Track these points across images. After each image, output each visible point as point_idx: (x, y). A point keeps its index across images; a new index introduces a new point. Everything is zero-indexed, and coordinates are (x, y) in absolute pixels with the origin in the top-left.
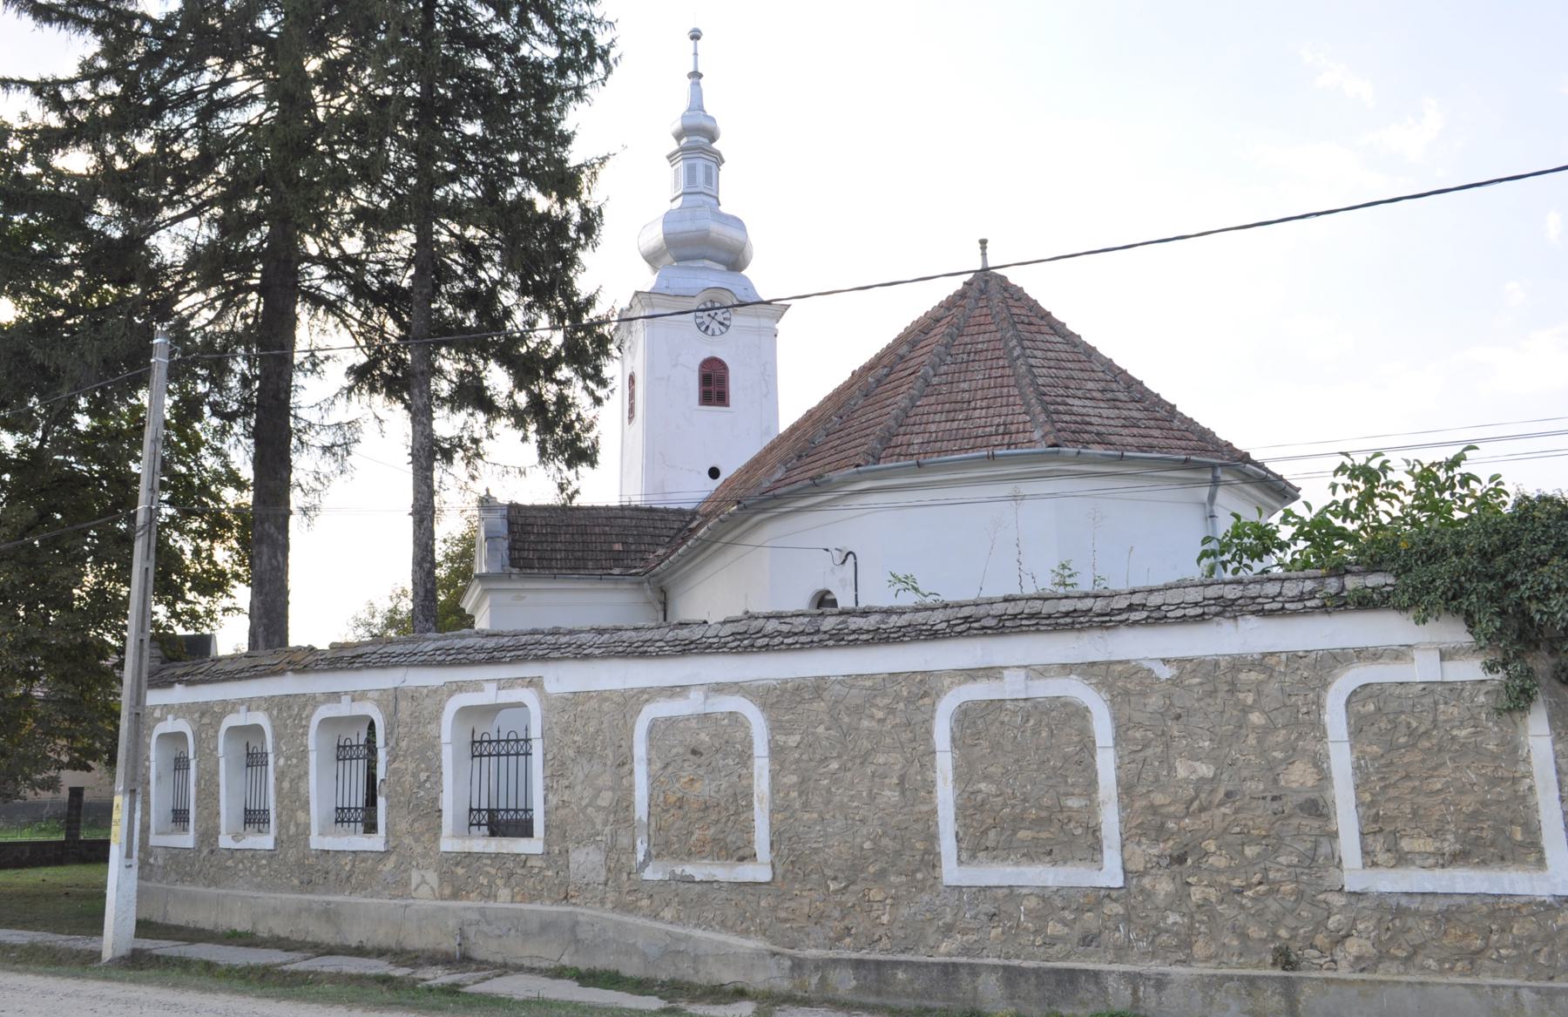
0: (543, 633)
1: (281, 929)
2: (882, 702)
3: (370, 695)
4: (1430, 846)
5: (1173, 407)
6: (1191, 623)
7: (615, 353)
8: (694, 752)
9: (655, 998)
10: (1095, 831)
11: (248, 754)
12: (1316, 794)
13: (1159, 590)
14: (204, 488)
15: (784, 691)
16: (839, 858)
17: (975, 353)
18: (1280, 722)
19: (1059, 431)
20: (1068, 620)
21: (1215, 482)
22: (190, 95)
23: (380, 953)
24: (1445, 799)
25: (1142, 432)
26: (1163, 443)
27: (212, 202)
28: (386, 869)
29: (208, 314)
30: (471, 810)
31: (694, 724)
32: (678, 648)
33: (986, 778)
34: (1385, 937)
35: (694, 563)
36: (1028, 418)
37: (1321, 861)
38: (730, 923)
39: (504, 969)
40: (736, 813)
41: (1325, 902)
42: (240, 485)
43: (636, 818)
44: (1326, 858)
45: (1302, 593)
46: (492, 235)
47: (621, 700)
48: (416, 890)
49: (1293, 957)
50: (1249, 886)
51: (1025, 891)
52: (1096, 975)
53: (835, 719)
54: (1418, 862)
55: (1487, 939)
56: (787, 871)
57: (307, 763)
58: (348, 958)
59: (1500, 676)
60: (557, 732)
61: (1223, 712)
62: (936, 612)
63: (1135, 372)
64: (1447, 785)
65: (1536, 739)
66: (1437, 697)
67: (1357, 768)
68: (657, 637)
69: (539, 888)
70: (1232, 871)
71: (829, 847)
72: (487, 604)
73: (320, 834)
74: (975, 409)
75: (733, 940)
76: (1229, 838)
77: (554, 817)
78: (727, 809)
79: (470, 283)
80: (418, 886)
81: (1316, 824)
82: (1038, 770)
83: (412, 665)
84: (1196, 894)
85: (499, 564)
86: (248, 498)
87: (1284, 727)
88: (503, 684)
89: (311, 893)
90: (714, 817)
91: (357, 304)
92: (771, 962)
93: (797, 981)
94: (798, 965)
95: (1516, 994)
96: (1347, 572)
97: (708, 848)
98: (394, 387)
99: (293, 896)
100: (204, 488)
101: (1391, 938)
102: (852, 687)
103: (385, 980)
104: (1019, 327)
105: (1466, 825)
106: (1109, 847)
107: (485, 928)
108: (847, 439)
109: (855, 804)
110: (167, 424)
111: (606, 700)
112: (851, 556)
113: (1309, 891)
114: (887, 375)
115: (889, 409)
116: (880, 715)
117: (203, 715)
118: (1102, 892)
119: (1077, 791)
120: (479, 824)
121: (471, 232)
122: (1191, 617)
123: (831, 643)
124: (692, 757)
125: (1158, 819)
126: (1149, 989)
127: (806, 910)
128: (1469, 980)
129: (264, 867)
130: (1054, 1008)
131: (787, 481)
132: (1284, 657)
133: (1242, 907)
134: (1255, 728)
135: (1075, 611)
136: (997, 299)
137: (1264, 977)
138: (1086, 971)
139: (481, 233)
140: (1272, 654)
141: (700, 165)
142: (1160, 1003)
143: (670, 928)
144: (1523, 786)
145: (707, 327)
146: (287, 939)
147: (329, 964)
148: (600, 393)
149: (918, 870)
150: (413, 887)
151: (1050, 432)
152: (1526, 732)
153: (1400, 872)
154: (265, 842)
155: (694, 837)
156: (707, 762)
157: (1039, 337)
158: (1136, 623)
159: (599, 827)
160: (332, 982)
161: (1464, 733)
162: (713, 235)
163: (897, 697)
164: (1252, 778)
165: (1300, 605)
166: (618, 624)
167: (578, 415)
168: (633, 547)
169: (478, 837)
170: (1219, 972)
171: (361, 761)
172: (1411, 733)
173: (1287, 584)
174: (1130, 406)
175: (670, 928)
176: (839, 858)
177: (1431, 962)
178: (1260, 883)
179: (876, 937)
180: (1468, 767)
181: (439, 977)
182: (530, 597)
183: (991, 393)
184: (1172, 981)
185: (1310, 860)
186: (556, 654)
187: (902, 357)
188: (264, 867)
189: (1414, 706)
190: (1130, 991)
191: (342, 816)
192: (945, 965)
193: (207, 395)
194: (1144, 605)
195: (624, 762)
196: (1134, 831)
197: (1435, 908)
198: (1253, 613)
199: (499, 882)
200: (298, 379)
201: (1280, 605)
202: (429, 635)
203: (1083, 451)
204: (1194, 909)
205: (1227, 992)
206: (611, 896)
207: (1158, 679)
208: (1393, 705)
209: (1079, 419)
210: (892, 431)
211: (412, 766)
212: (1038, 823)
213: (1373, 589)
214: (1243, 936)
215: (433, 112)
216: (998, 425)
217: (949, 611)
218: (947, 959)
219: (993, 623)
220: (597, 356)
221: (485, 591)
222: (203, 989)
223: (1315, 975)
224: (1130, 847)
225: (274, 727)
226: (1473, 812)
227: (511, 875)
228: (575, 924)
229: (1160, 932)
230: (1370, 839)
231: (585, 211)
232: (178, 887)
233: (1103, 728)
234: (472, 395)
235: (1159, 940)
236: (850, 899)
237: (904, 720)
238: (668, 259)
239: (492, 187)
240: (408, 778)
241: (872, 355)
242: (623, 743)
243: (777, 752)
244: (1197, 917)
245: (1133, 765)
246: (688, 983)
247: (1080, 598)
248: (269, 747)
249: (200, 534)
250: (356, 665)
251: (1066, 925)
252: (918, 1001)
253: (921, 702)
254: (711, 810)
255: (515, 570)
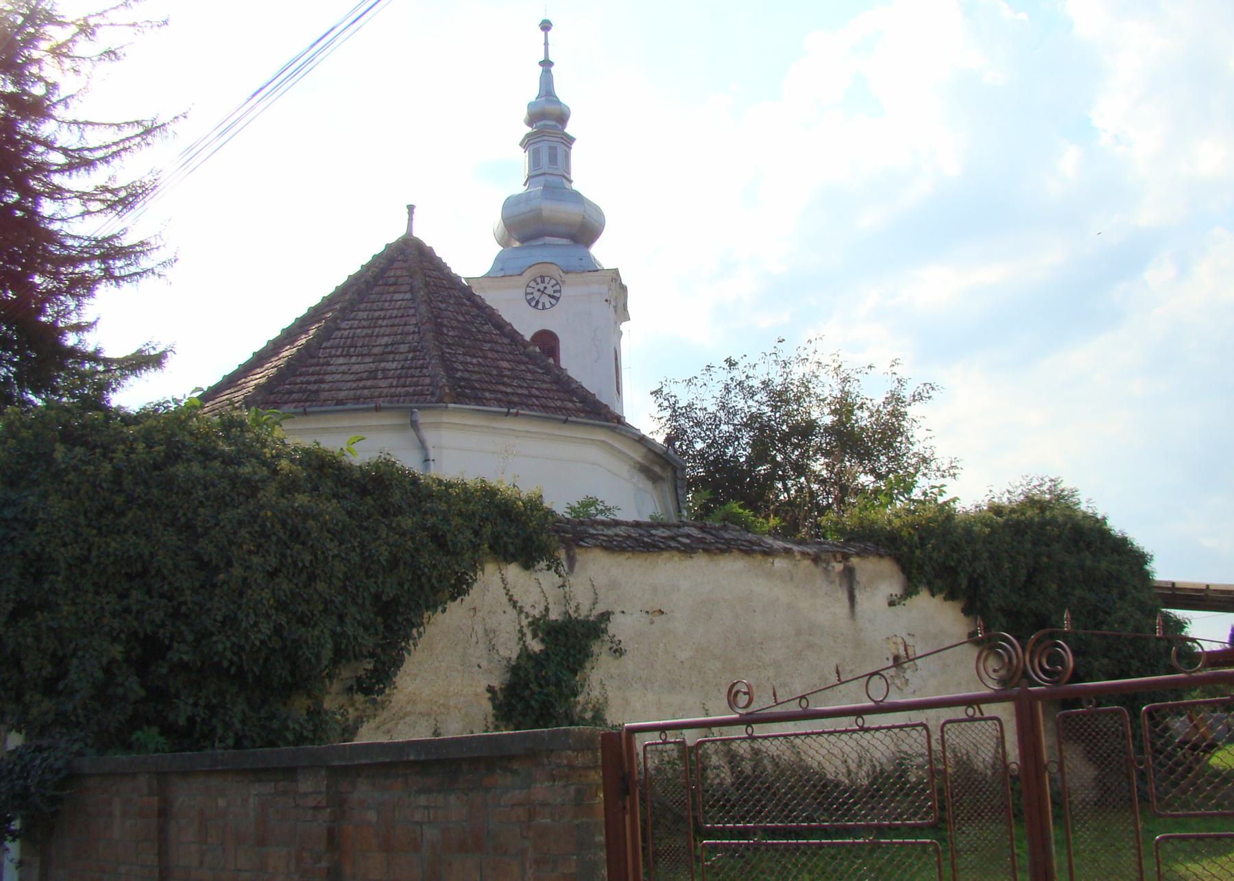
49: (359, 697)
124: (477, 668)
145: (537, 302)
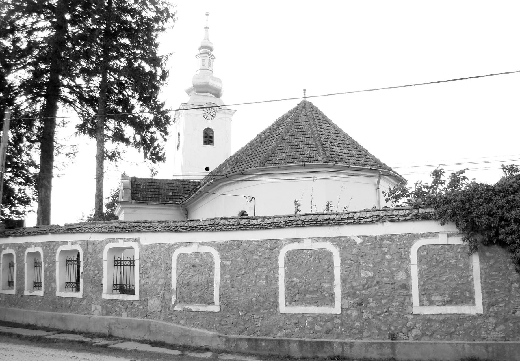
0: (140, 222)
1: (45, 323)
2: (261, 250)
3: (78, 242)
4: (440, 298)
5: (367, 151)
6: (368, 224)
7: (172, 123)
8: (193, 266)
9: (177, 351)
10: (332, 295)
11: (35, 262)
12: (406, 282)
13: (358, 212)
14: (22, 167)
15: (226, 245)
16: (244, 304)
17: (300, 129)
18: (396, 258)
19: (328, 157)
20: (327, 222)
21: (380, 176)
22: (24, 26)
23: (81, 333)
24: (446, 283)
25: (356, 159)
26: (363, 163)
27: (30, 64)
28: (83, 304)
29: (27, 104)
30: (113, 284)
31: (194, 256)
32: (189, 229)
33: (296, 276)
34: (424, 329)
35: (197, 200)
36: (317, 152)
37: (406, 304)
38: (204, 326)
39: (124, 340)
40: (208, 288)
41: (406, 318)
42: (36, 167)
43: (172, 289)
44: (408, 303)
45: (405, 214)
46: (130, 80)
47: (168, 247)
48: (93, 312)
50: (383, 313)
51: (308, 315)
52: (330, 343)
53: (244, 256)
54: (437, 304)
55: (456, 328)
56: (225, 308)
57: (56, 266)
58: (69, 334)
59: (467, 243)
60: (144, 258)
61: (377, 254)
62: (281, 219)
63: (355, 138)
64: (447, 279)
65: (475, 263)
66: (446, 249)
67: (419, 273)
68: (181, 225)
69: (137, 312)
70: (377, 308)
71: (240, 300)
72: (123, 212)
73: (60, 291)
74: (299, 148)
75: (205, 332)
76: (377, 297)
77: (143, 288)
78: (204, 286)
79: (121, 96)
80: (94, 310)
81: (405, 292)
82: (314, 274)
83: (93, 232)
84: (365, 316)
85: (128, 198)
86: (37, 171)
87: (397, 259)
88: (126, 240)
89: (56, 311)
90: (200, 289)
91: (80, 103)
92: (219, 339)
93: (227, 346)
94: (228, 340)
95: (463, 345)
96: (420, 207)
97: (197, 300)
98: (92, 133)
99: (51, 313)
100: (22, 167)
101: (426, 329)
102: (250, 244)
103: (82, 342)
104: (316, 120)
105: (452, 292)
106: (337, 300)
107: (118, 326)
108: (254, 157)
109: (250, 285)
110: (10, 144)
111: (162, 247)
112: (253, 199)
113: (402, 314)
114: (269, 135)
115: (269, 147)
116: (260, 254)
117: (19, 248)
118: (334, 316)
119: (327, 281)
120: (116, 290)
121: (122, 78)
122: (368, 222)
123: (244, 228)
124: (193, 268)
125: (354, 291)
126: (347, 347)
127: (231, 322)
128: (449, 342)
129: (40, 302)
130: (315, 354)
131: (232, 172)
132: (398, 236)
133: (380, 320)
134: (388, 260)
135: (329, 219)
136: (308, 110)
137: (386, 342)
138: (327, 342)
139: (126, 79)
140: (394, 235)
141: (207, 59)
142: (351, 352)
143: (183, 327)
144: (470, 279)
145: (207, 117)
146: (48, 327)
147: (62, 336)
148: (166, 137)
149: (271, 308)
150: (92, 311)
151: (324, 157)
152: (472, 261)
153: (431, 307)
154: (41, 293)
155: (192, 296)
156: (198, 270)
157: (322, 124)
158: (350, 223)
159: (159, 291)
160: (63, 342)
161: (453, 261)
162: (210, 84)
163: (266, 248)
164: (385, 277)
165: (404, 218)
166: (168, 220)
167: (158, 144)
168: (176, 194)
169: (116, 294)
170: (371, 341)
171: (75, 266)
172: (437, 261)
173: (400, 211)
174: (352, 149)
175: (183, 327)
176: (244, 304)
177: (438, 336)
178: (386, 312)
179: (256, 331)
180: (454, 273)
181: (101, 342)
182: (138, 211)
183: (305, 143)
184: (355, 345)
185: (403, 304)
186: (145, 230)
187: (274, 129)
188: (40, 302)
189: (438, 252)
190: (341, 348)
191: (68, 285)
192: (279, 340)
193: (25, 133)
194: (353, 217)
195: (168, 269)
196: (345, 295)
197: (441, 319)
198: (389, 221)
199: (123, 310)
200: (57, 129)
201: (398, 218)
202: (100, 222)
203: (336, 164)
204: (364, 321)
205: (373, 348)
206: (163, 316)
207: (356, 243)
208: (432, 252)
209: (335, 153)
210: (270, 155)
211: (92, 268)
212: (313, 292)
213: (428, 213)
214: (380, 329)
215: (110, 35)
216: (307, 154)
217: (286, 218)
218: (280, 338)
219: (301, 222)
220: (165, 124)
221: (122, 208)
222: (15, 343)
223: (402, 341)
224: (344, 300)
225: (44, 253)
226: (455, 287)
227: (127, 307)
228: (150, 325)
229: (352, 328)
230: (422, 297)
231: (163, 71)
232: (9, 308)
233: (337, 260)
234: (118, 136)
235: (352, 331)
236: (247, 318)
237: (268, 256)
238: (194, 92)
239: (130, 64)
240: (91, 273)
241: (265, 129)
242: (168, 262)
243: (223, 267)
244: (365, 323)
245: (347, 272)
246: (189, 346)
247: (331, 214)
248: (42, 260)
249: (21, 183)
250: (73, 232)
251: (321, 327)
252: (269, 352)
253: (274, 250)
254: (199, 286)
255: (134, 201)
